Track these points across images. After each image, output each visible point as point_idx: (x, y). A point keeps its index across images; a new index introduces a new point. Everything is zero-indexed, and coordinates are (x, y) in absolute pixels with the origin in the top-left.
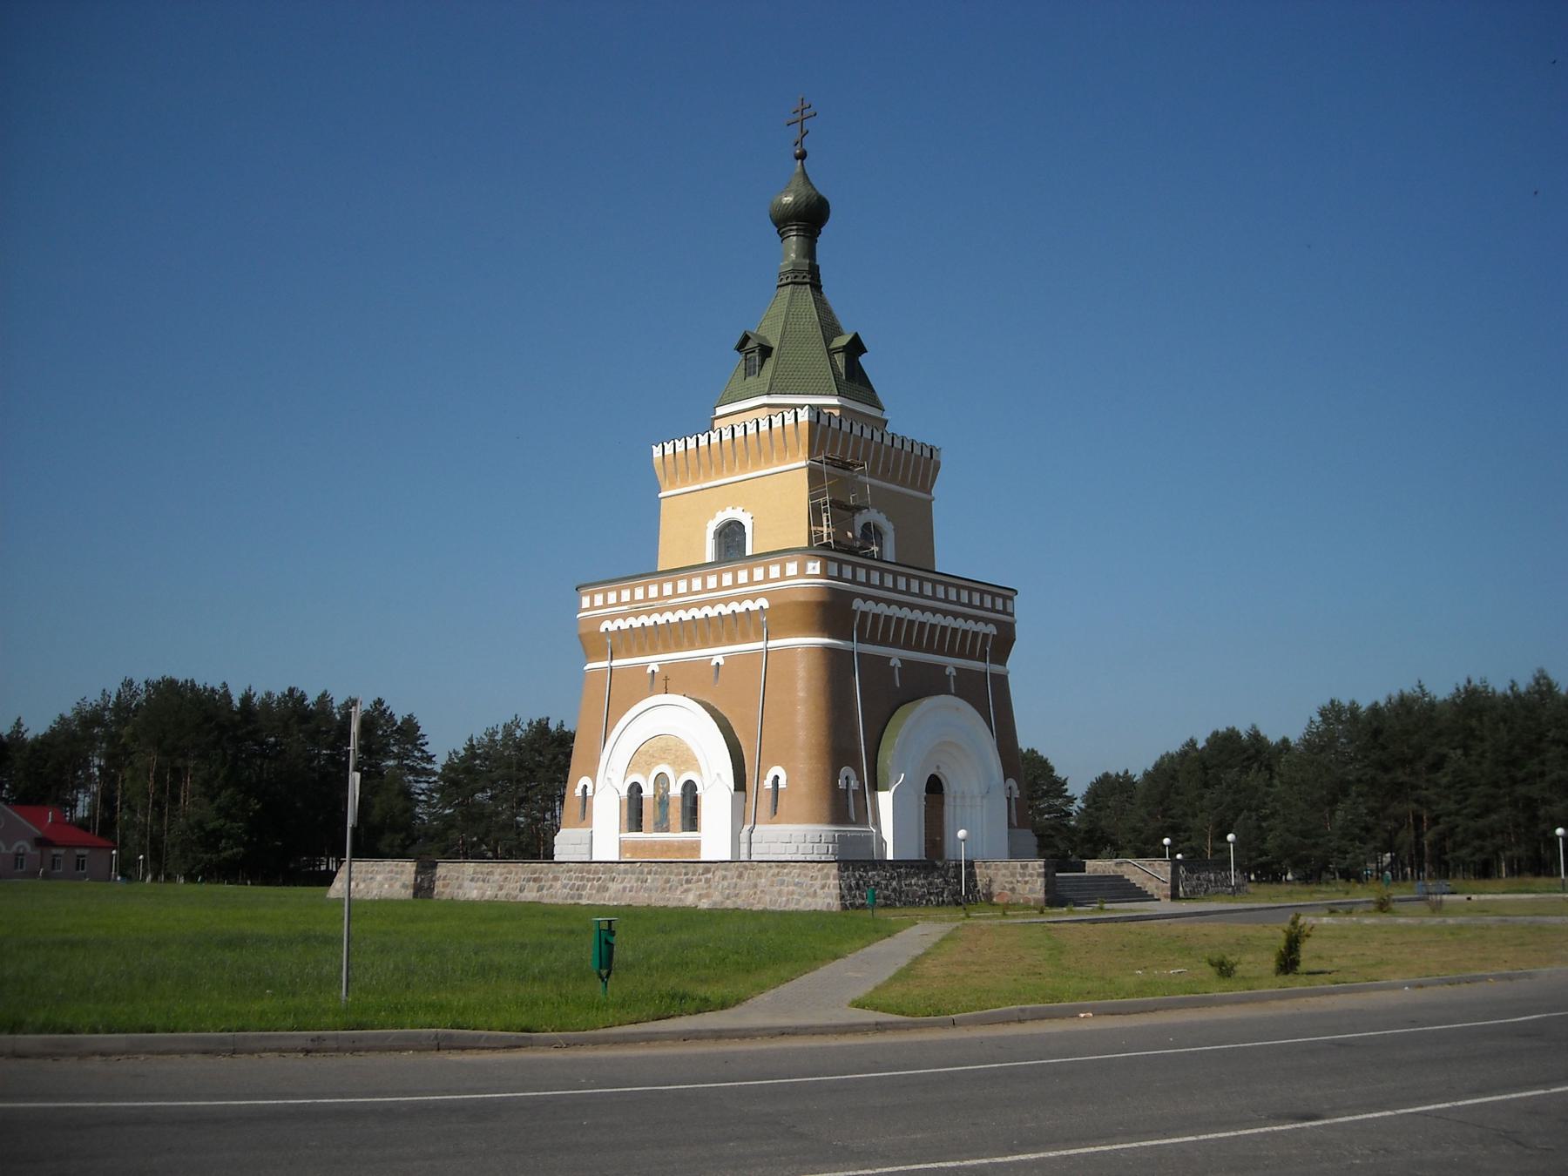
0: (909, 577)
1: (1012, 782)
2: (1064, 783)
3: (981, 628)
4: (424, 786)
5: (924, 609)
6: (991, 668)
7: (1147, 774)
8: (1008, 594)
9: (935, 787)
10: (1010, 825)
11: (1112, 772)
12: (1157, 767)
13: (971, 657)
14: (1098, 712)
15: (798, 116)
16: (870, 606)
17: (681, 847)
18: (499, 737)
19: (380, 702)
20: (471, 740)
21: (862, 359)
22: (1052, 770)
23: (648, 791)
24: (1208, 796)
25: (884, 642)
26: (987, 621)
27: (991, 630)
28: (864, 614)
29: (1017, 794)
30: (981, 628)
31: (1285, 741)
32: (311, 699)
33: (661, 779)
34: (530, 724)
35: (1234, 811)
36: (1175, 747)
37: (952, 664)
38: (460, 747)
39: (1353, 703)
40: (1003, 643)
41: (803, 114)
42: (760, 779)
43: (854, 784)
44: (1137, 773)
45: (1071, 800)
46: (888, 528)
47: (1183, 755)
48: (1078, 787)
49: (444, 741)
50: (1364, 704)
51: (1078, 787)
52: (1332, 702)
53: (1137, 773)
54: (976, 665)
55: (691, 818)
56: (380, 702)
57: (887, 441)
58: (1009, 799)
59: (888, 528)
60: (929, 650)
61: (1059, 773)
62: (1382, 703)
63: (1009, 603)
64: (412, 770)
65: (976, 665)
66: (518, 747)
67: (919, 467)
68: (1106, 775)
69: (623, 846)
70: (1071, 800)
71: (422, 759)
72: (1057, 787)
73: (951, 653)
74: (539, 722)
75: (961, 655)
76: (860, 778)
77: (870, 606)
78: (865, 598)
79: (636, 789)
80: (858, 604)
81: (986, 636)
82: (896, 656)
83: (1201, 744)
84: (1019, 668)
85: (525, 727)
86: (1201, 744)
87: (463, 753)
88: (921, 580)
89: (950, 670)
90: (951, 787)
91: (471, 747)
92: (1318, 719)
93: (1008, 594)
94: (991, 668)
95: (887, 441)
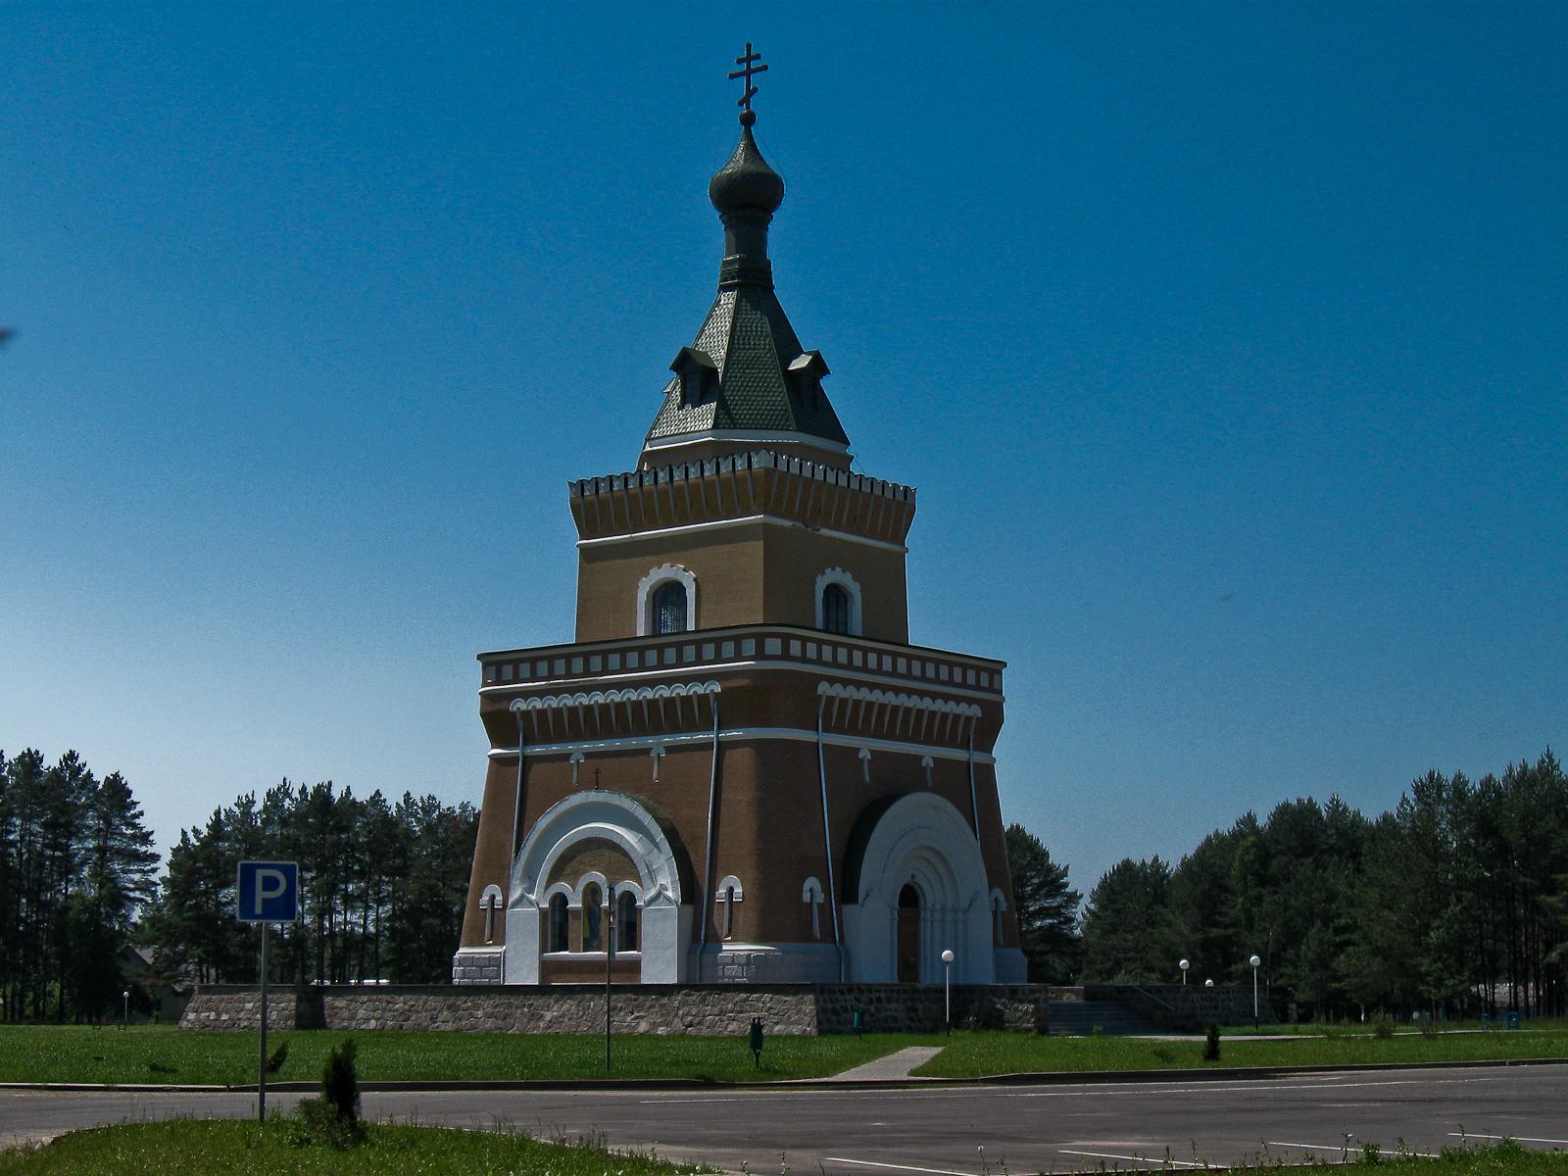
0: (880, 653)
1: (998, 893)
2: (1065, 873)
3: (963, 709)
4: (137, 877)
5: (897, 690)
6: (978, 757)
7: (1186, 865)
8: (994, 668)
9: (910, 898)
10: (996, 944)
11: (1137, 860)
12: (1201, 853)
13: (952, 744)
14: (1107, 785)
15: (744, 67)
16: (837, 691)
17: (611, 966)
18: (258, 807)
19: (72, 756)
20: (218, 813)
21: (824, 383)
22: (1045, 855)
23: (575, 903)
24: (1267, 899)
25: (852, 731)
26: (970, 701)
27: (975, 711)
28: (830, 700)
29: (1004, 906)
30: (963, 709)
31: (1386, 817)
32: (51, 761)
33: (592, 891)
34: (303, 791)
35: (1276, 933)
36: (1227, 825)
37: (928, 753)
38: (202, 821)
39: (1459, 776)
40: (991, 721)
41: (750, 64)
42: (713, 889)
43: (820, 898)
44: (1172, 862)
45: (1073, 898)
46: (854, 589)
47: (1237, 836)
48: (1084, 879)
49: (173, 813)
50: (1474, 781)
51: (1084, 879)
52: (1431, 775)
53: (1172, 862)
54: (959, 755)
55: (631, 936)
56: (72, 756)
57: (855, 485)
58: (995, 913)
59: (854, 589)
60: (903, 738)
61: (1056, 859)
62: (1499, 777)
63: (996, 676)
64: (120, 853)
65: (959, 755)
66: (284, 823)
67: (892, 511)
68: (1127, 866)
69: (547, 968)
70: (1073, 898)
71: (133, 837)
72: (1053, 881)
73: (927, 741)
74: (318, 789)
75: (939, 743)
76: (826, 890)
77: (837, 691)
78: (832, 680)
79: (560, 900)
80: (824, 688)
81: (968, 719)
82: (866, 746)
83: (1262, 821)
84: (1005, 754)
85: (296, 795)
86: (1262, 821)
87: (205, 832)
88: (895, 655)
89: (927, 762)
90: (932, 897)
91: (216, 825)
92: (1411, 796)
93: (994, 668)
94: (978, 757)
95: (855, 485)
